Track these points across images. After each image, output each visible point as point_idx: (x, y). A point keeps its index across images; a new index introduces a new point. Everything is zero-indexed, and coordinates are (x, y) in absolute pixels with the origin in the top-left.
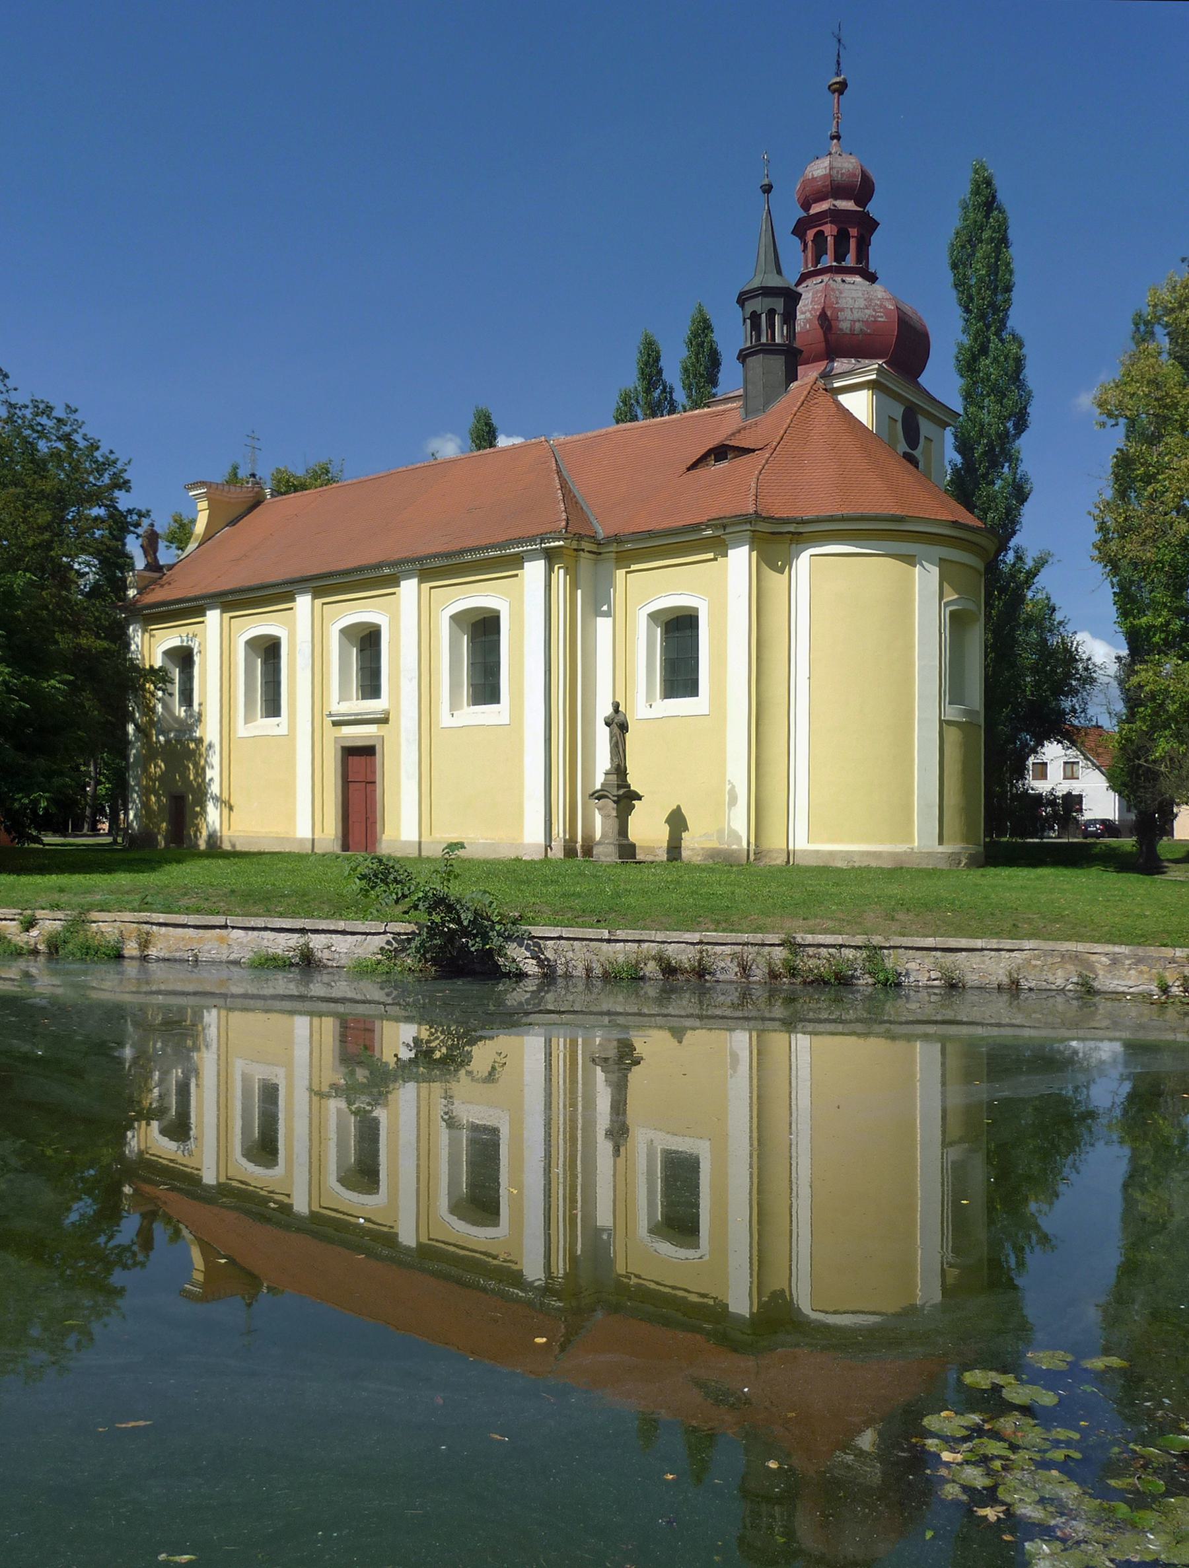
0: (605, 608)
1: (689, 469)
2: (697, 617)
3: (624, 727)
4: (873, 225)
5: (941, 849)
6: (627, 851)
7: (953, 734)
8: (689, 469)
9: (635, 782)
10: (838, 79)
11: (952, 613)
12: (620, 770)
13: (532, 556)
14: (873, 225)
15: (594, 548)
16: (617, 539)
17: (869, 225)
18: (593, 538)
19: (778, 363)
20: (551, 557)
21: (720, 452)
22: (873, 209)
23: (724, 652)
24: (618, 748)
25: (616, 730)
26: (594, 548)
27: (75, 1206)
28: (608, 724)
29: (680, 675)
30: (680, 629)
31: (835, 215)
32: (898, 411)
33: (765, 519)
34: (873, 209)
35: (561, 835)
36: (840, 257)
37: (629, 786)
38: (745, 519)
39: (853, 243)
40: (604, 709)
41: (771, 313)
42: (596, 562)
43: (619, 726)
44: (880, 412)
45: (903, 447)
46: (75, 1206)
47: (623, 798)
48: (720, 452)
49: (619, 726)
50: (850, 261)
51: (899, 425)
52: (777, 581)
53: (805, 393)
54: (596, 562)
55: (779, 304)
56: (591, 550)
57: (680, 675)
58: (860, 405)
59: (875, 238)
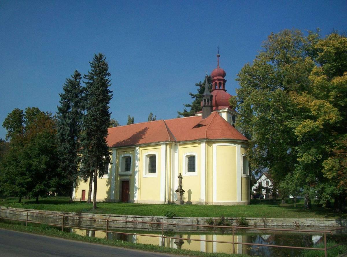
0: (176, 152)
1: (193, 128)
2: (195, 157)
3: (182, 178)
4: (225, 81)
5: (242, 202)
6: (182, 202)
7: (244, 179)
8: (193, 128)
9: (183, 189)
10: (218, 55)
11: (243, 156)
12: (181, 186)
13: (163, 144)
14: (225, 81)
15: (175, 143)
16: (180, 142)
17: (225, 81)
18: (175, 142)
19: (209, 108)
20: (167, 145)
21: (199, 126)
22: (225, 78)
23: (200, 163)
24: (180, 182)
25: (180, 179)
26: (175, 143)
27: (24, 176)
28: (178, 177)
29: (192, 167)
30: (192, 160)
31: (219, 80)
32: (231, 116)
33: (208, 139)
34: (225, 78)
35: (168, 199)
36: (219, 87)
37: (182, 190)
38: (204, 139)
39: (222, 84)
40: (177, 175)
41: (208, 99)
42: (175, 146)
43: (180, 177)
44: (229, 117)
45: (232, 123)
46: (24, 176)
47: (182, 192)
48: (199, 126)
49: (180, 177)
50: (221, 87)
51: (232, 119)
52: (210, 148)
53: (215, 115)
54: (175, 146)
55: (209, 98)
56: (174, 141)
57: (192, 167)
58: (225, 116)
59: (226, 83)
